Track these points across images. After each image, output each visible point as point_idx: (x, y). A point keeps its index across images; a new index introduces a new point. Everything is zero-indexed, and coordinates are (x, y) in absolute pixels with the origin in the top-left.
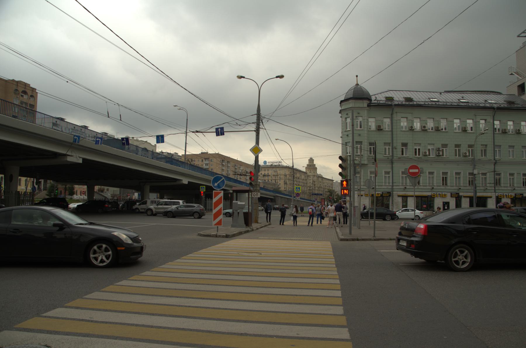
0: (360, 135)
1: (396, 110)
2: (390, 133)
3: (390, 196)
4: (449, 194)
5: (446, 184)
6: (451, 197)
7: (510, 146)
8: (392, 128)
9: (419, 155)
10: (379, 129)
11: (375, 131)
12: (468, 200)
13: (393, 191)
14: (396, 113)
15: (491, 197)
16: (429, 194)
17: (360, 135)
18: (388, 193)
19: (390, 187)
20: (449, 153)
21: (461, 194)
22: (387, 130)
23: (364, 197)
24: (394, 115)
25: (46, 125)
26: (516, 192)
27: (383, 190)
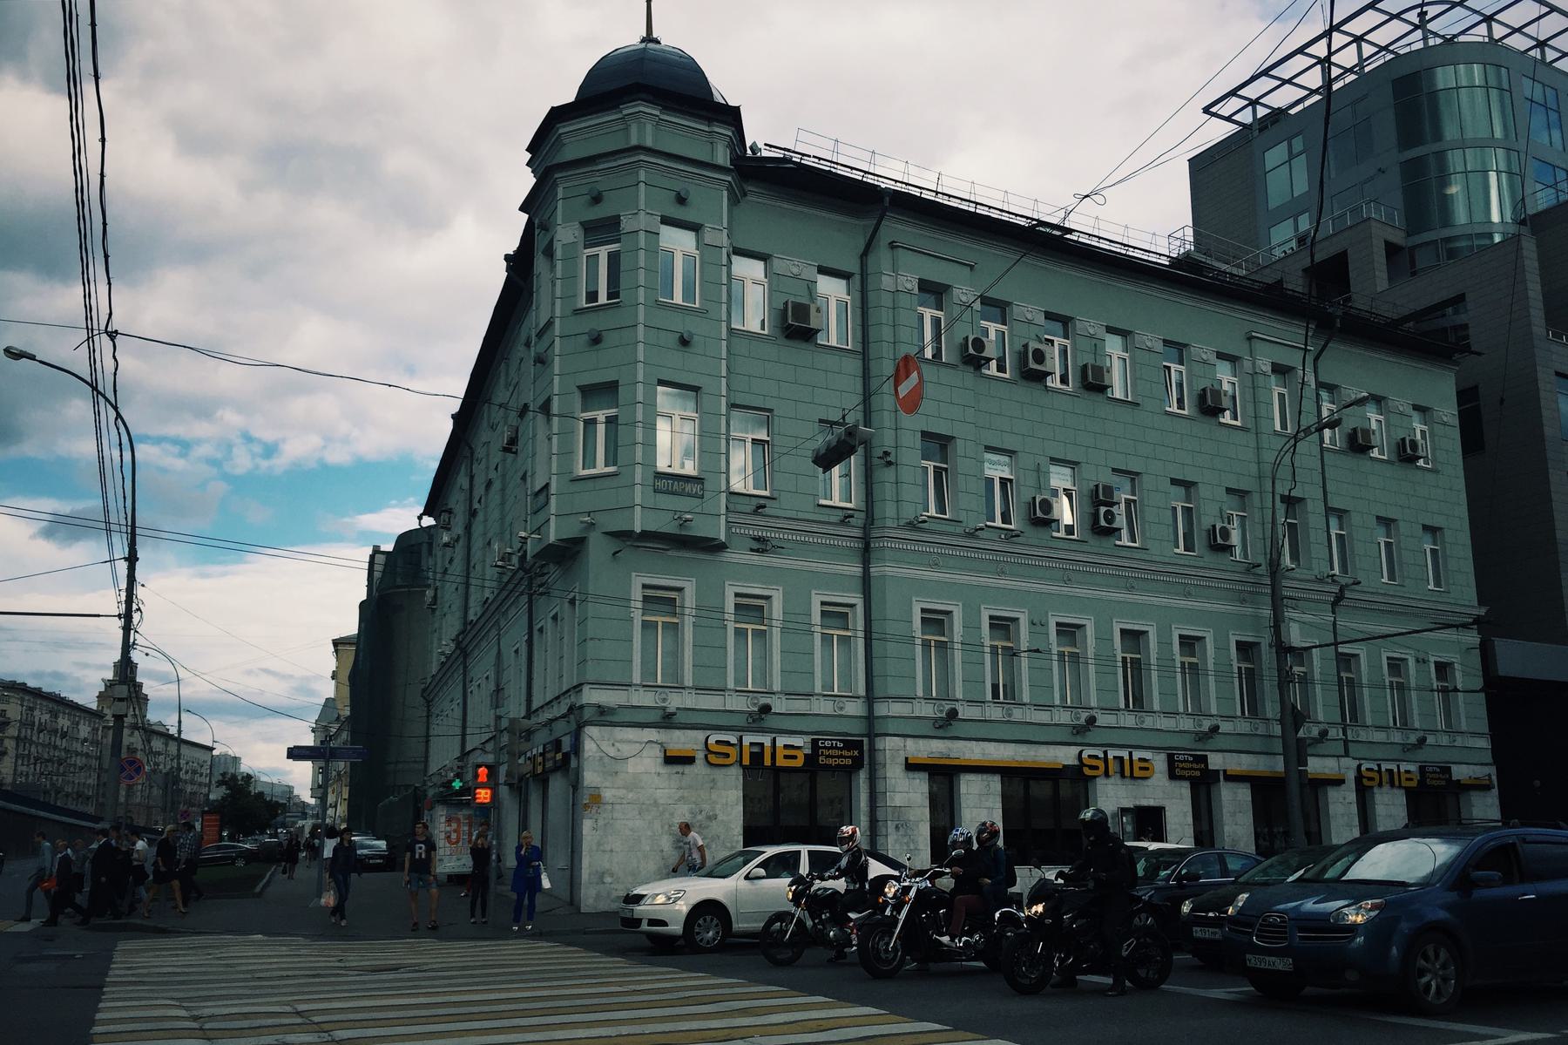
0: (684, 342)
1: (895, 228)
2: (854, 365)
3: (858, 764)
4: (1159, 762)
5: (1139, 701)
6: (1173, 776)
7: (1381, 520)
8: (865, 340)
9: (1006, 518)
10: (795, 326)
11: (1182, 276)
12: (1244, 793)
13: (872, 735)
14: (893, 246)
15: (1339, 782)
16: (1065, 756)
17: (684, 342)
18: (849, 745)
19: (855, 708)
20: (1156, 532)
21: (1216, 761)
22: (833, 342)
23: (699, 768)
24: (882, 258)
25: (1226, 828)
26: (1424, 755)
27: (815, 725)
